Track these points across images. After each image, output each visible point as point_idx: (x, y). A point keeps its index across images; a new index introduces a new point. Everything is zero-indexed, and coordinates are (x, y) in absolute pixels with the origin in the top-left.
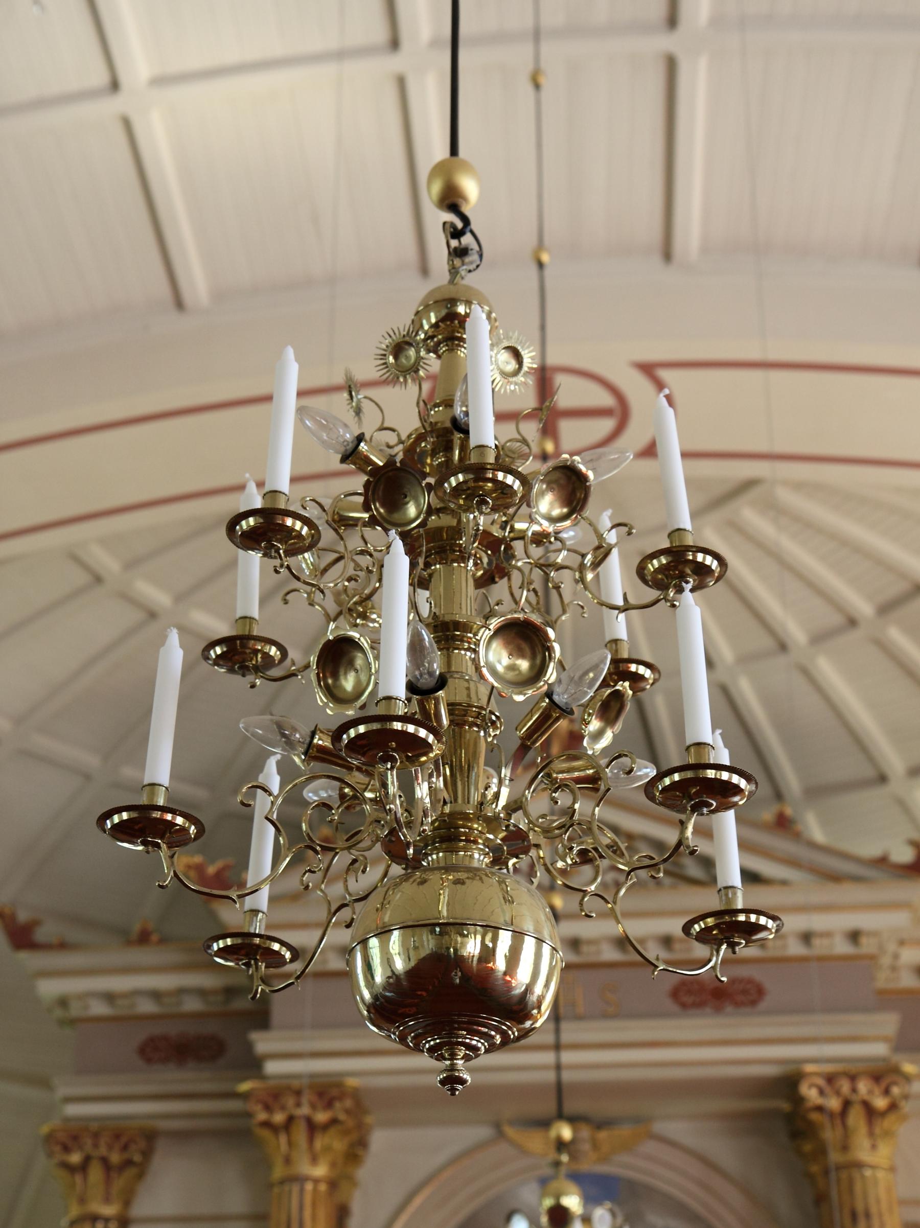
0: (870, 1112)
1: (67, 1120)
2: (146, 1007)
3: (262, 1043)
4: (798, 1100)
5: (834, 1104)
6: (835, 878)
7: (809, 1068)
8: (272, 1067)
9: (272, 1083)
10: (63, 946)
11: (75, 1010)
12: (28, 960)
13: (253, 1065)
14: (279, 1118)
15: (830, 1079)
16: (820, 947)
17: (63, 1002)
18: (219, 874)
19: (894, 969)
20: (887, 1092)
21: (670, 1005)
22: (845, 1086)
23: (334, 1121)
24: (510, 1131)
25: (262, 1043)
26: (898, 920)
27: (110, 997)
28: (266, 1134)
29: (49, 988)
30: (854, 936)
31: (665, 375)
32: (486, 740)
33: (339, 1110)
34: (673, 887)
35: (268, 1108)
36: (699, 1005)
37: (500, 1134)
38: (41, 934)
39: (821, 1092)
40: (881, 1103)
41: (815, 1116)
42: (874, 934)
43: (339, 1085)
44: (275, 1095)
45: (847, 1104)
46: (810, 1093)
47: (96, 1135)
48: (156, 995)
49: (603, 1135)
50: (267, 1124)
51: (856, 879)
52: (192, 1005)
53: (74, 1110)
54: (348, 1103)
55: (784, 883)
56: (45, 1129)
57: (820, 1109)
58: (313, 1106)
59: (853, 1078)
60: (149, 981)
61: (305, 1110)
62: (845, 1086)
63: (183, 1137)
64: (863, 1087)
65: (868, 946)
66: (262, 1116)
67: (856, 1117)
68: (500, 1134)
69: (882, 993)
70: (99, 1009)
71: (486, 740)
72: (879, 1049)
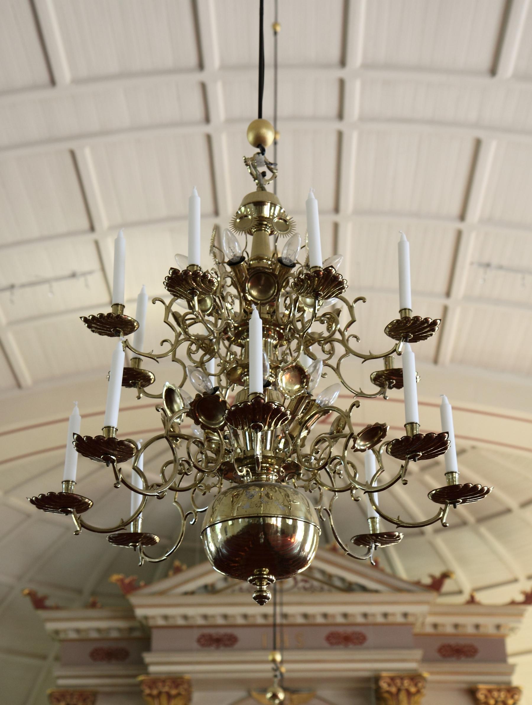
0: (409, 694)
1: (59, 686)
2: (94, 635)
3: (148, 658)
4: (378, 689)
5: (394, 690)
6: (399, 590)
7: (384, 674)
8: (152, 669)
9: (152, 676)
10: (57, 608)
11: (62, 636)
12: (42, 614)
13: (143, 666)
14: (155, 692)
15: (393, 679)
16: (391, 619)
17: (57, 632)
18: (130, 584)
19: (423, 624)
20: (416, 685)
21: (326, 644)
22: (398, 682)
23: (179, 694)
24: (254, 694)
25: (148, 658)
26: (424, 608)
27: (78, 631)
28: (149, 699)
29: (51, 626)
30: (405, 615)
31: (335, 367)
32: (221, 289)
33: (181, 690)
34: (330, 591)
35: (150, 688)
36: (338, 643)
37: (250, 695)
38: (48, 603)
39: (389, 685)
40: (413, 690)
41: (386, 695)
42: (414, 615)
43: (182, 678)
44: (154, 682)
45: (399, 690)
46: (384, 685)
47: (72, 695)
48: (99, 630)
49: (295, 697)
50: (150, 695)
51: (408, 591)
52: (114, 634)
53: (61, 682)
54: (186, 686)
55: (376, 591)
56: (49, 691)
57: (388, 692)
58: (170, 688)
59: (402, 678)
60: (97, 624)
61: (166, 689)
62: (398, 682)
63: (110, 694)
64: (406, 683)
65: (411, 619)
66: (147, 691)
67: (403, 696)
68: (250, 695)
69: (417, 635)
70: (73, 635)
71: (221, 289)
72: (412, 665)
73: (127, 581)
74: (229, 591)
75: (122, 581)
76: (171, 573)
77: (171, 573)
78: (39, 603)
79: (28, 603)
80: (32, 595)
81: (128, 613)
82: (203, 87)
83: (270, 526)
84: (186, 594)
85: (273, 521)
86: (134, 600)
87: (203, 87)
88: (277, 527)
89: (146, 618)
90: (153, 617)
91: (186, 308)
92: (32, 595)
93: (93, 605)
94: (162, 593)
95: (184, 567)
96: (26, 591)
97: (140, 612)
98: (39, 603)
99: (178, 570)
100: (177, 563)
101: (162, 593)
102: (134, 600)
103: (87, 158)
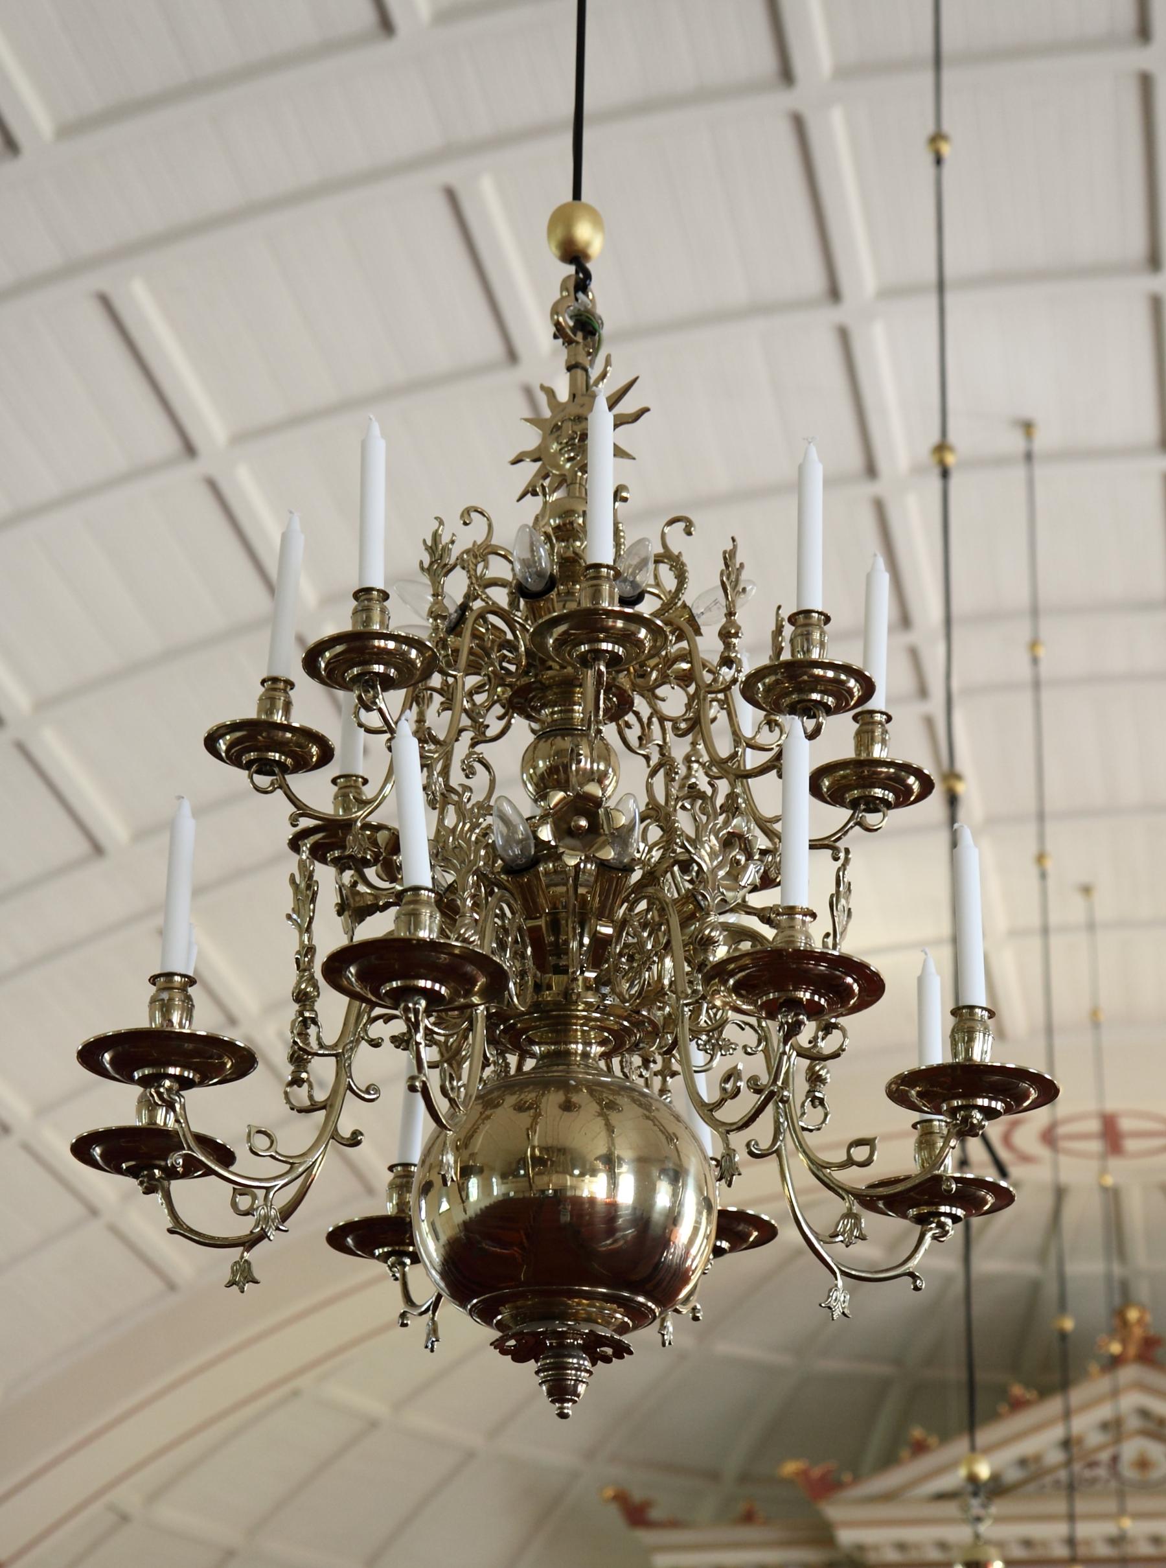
10: (673, 1524)
12: (647, 1537)
38: (655, 1514)
73: (816, 1472)
74: (1031, 1487)
75: (804, 1473)
76: (905, 1453)
77: (905, 1453)
78: (636, 1514)
79: (614, 1516)
80: (621, 1499)
81: (823, 1535)
82: (799, 123)
83: (583, 1208)
84: (941, 1497)
85: (595, 1187)
86: (833, 1511)
87: (799, 123)
88: (612, 1207)
89: (861, 1548)
90: (876, 1548)
91: (417, 612)
92: (621, 1499)
93: (748, 1518)
94: (888, 1497)
95: (933, 1440)
96: (609, 1492)
97: (847, 1537)
98: (636, 1514)
99: (920, 1448)
100: (917, 1433)
101: (888, 1497)
102: (833, 1511)
103: (141, 300)
